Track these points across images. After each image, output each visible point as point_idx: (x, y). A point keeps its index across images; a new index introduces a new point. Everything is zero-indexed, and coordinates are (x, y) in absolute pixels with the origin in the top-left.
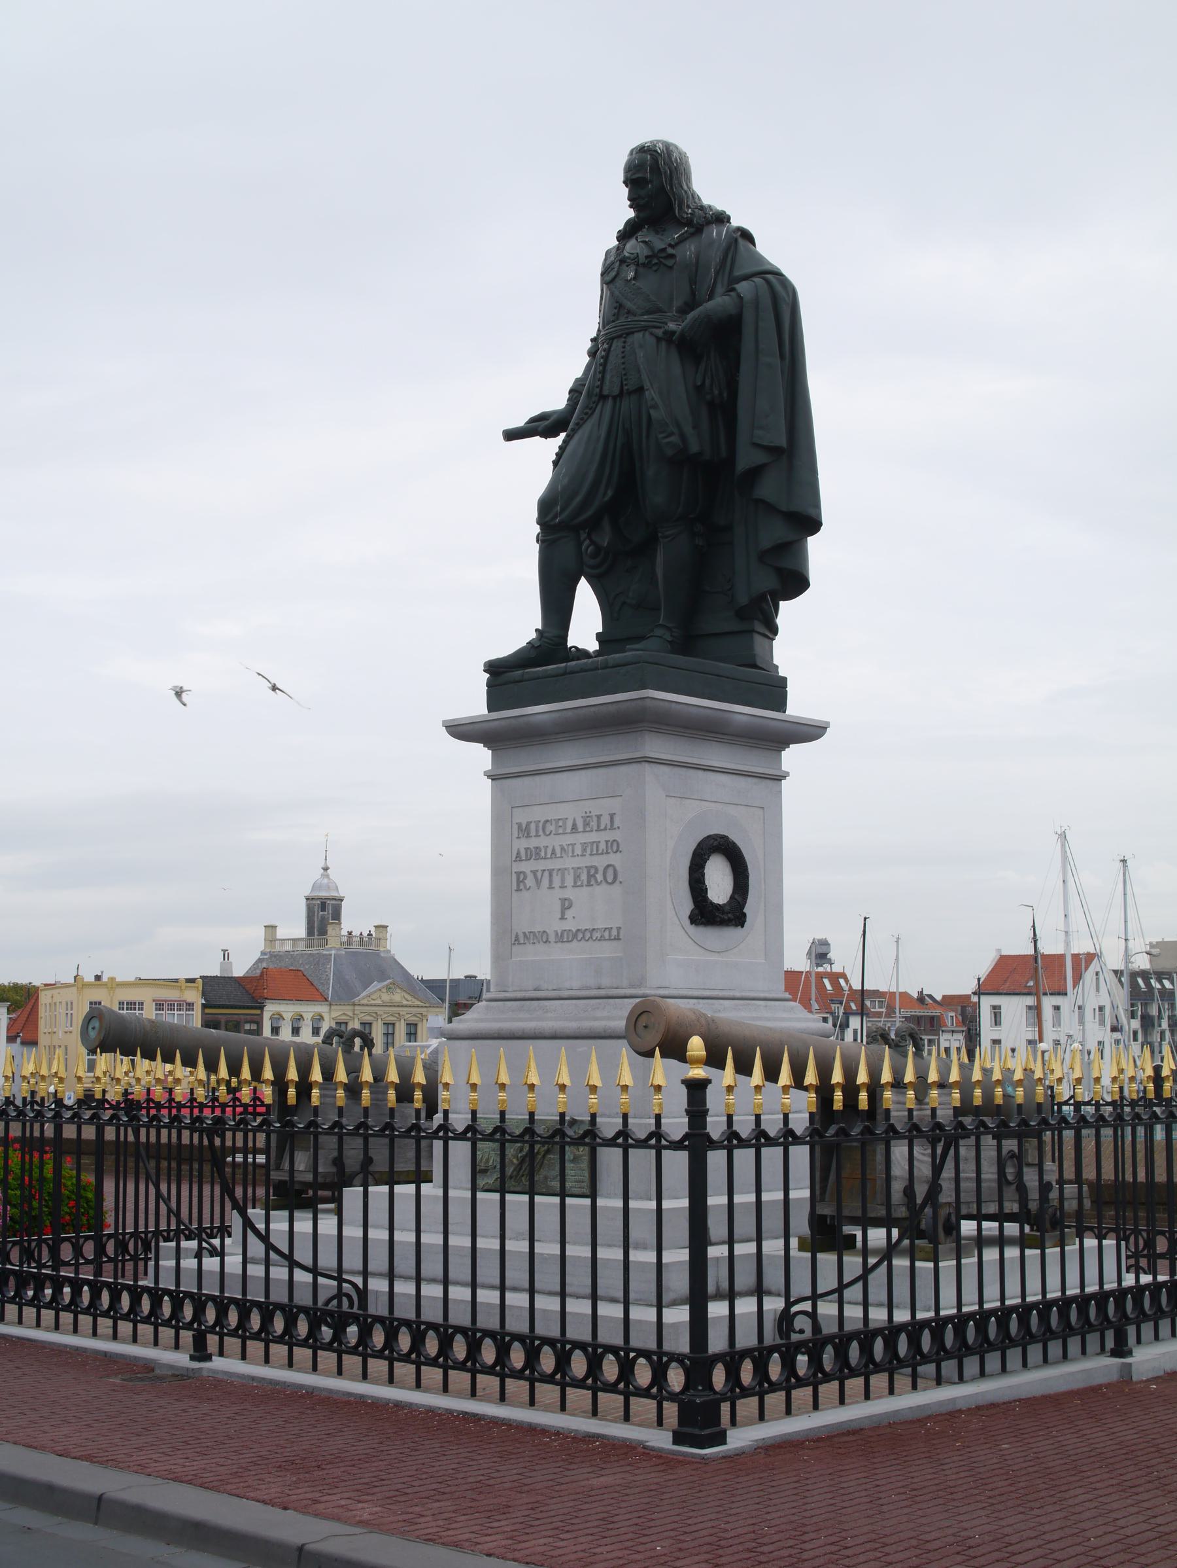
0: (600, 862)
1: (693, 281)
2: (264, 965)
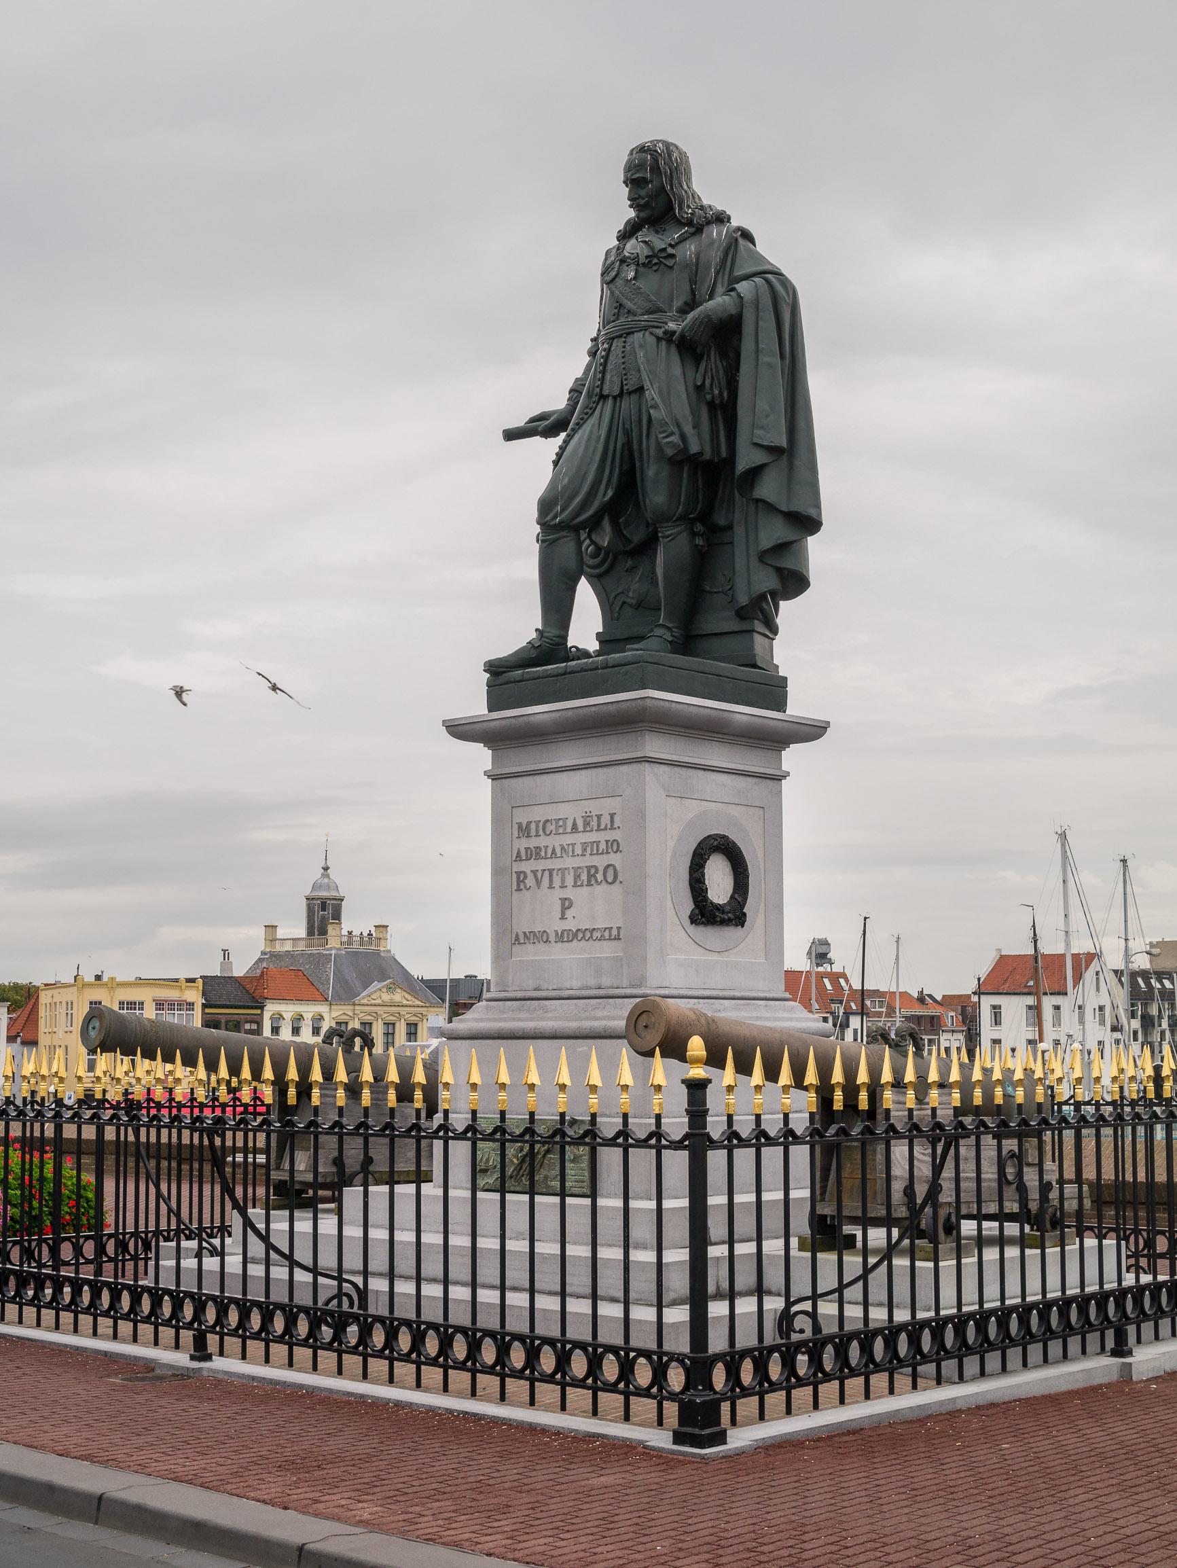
1: (693, 282)
2: (265, 965)
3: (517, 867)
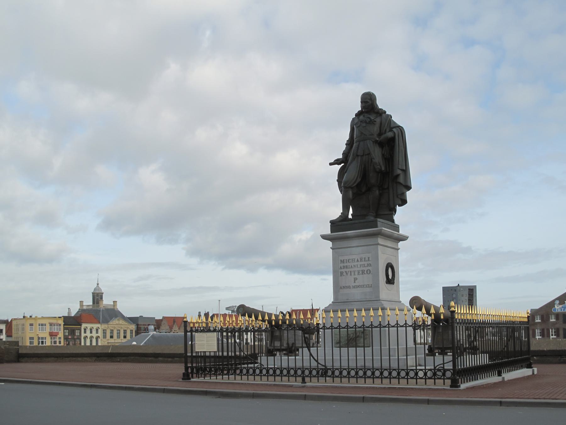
0: (366, 269)
3: (340, 270)
